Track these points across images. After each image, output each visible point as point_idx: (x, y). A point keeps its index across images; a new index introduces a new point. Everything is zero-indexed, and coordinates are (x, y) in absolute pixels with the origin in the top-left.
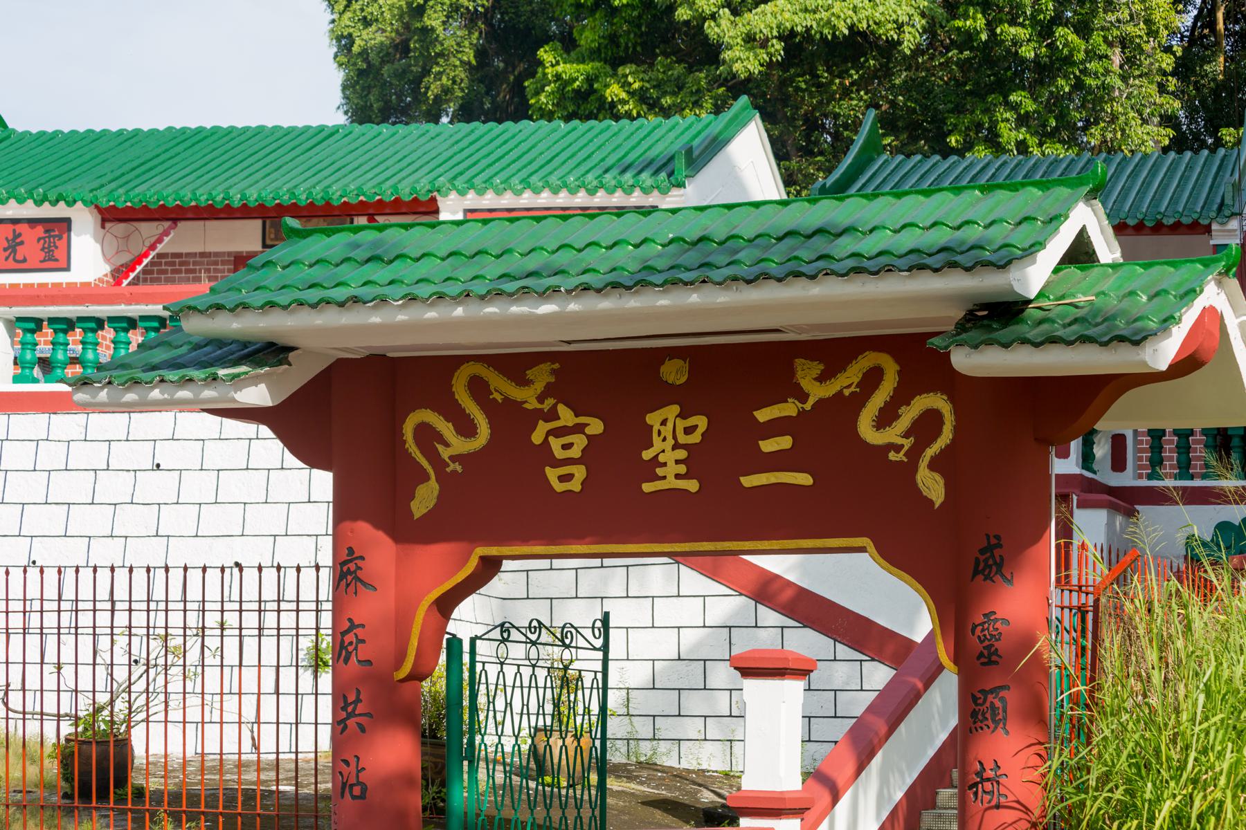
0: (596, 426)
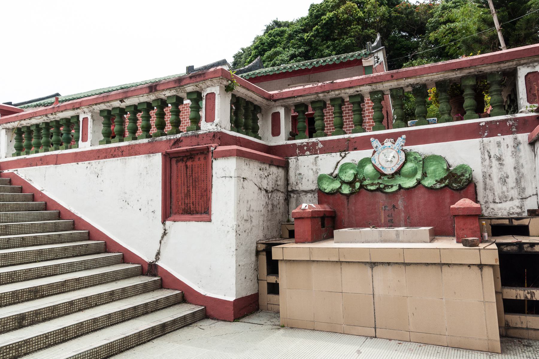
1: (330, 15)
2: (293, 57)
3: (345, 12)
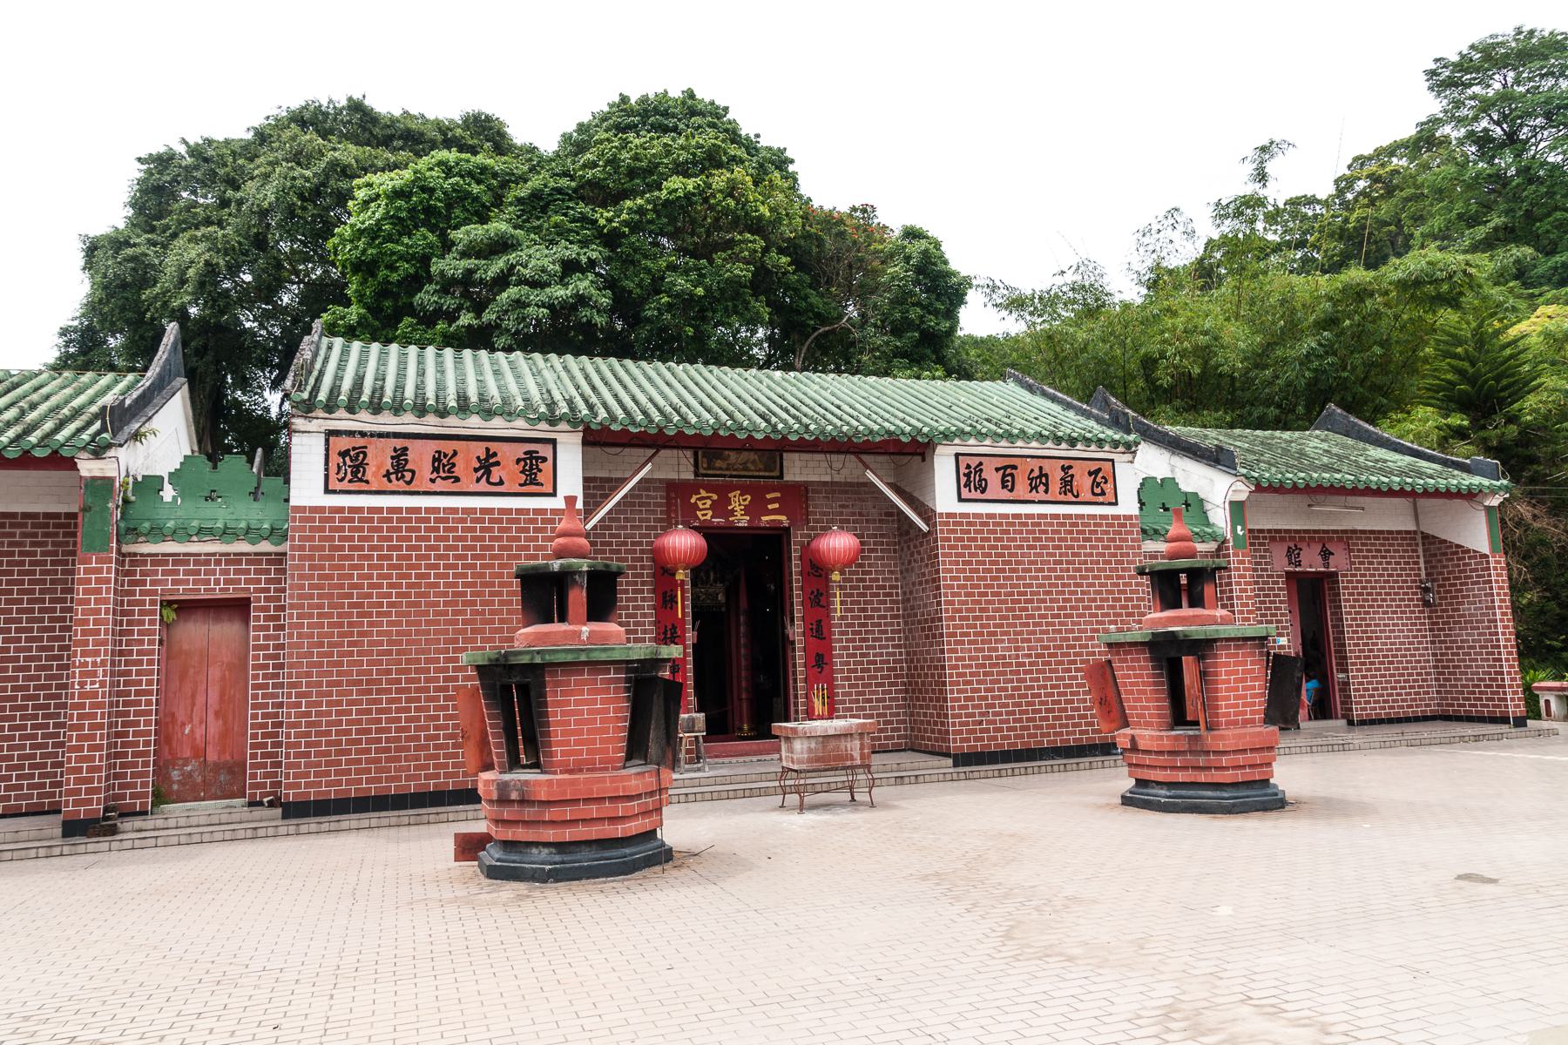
0: (715, 497)
1: (676, 184)
2: (570, 267)
3: (731, 190)
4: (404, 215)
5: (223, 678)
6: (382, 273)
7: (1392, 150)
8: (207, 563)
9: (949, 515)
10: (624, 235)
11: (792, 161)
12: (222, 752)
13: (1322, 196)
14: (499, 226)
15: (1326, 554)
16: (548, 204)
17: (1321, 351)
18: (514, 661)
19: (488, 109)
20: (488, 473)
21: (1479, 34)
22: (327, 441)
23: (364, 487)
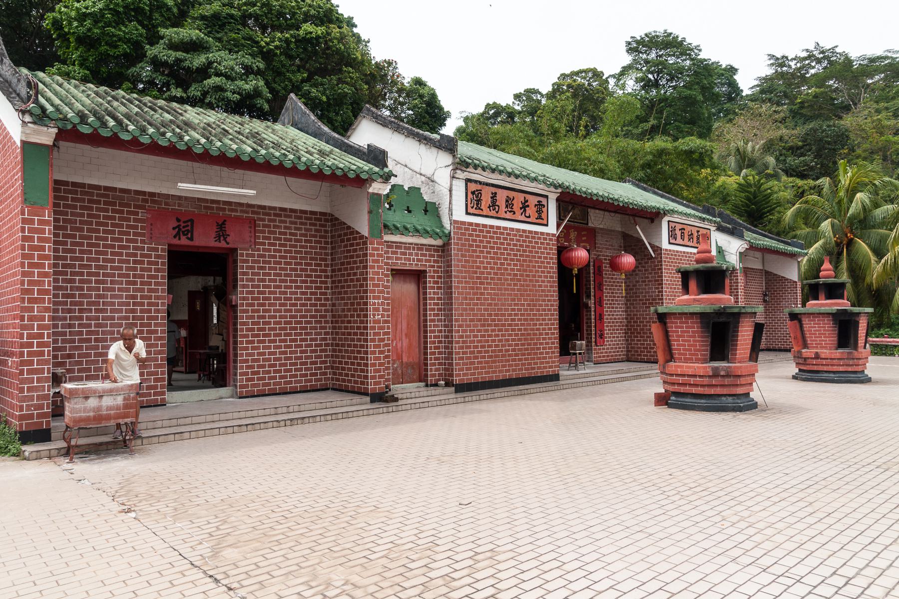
4: (121, 9)
5: (408, 315)
6: (104, 48)
7: (577, 73)
8: (409, 248)
9: (666, 250)
10: (276, 54)
11: (356, 26)
12: (409, 357)
13: (544, 92)
14: (190, 32)
15: (222, 233)
16: (224, 25)
17: (646, 179)
18: (729, 311)
19: (657, 26)
20: (525, 211)
21: (649, 29)
22: (466, 184)
23: (481, 213)
